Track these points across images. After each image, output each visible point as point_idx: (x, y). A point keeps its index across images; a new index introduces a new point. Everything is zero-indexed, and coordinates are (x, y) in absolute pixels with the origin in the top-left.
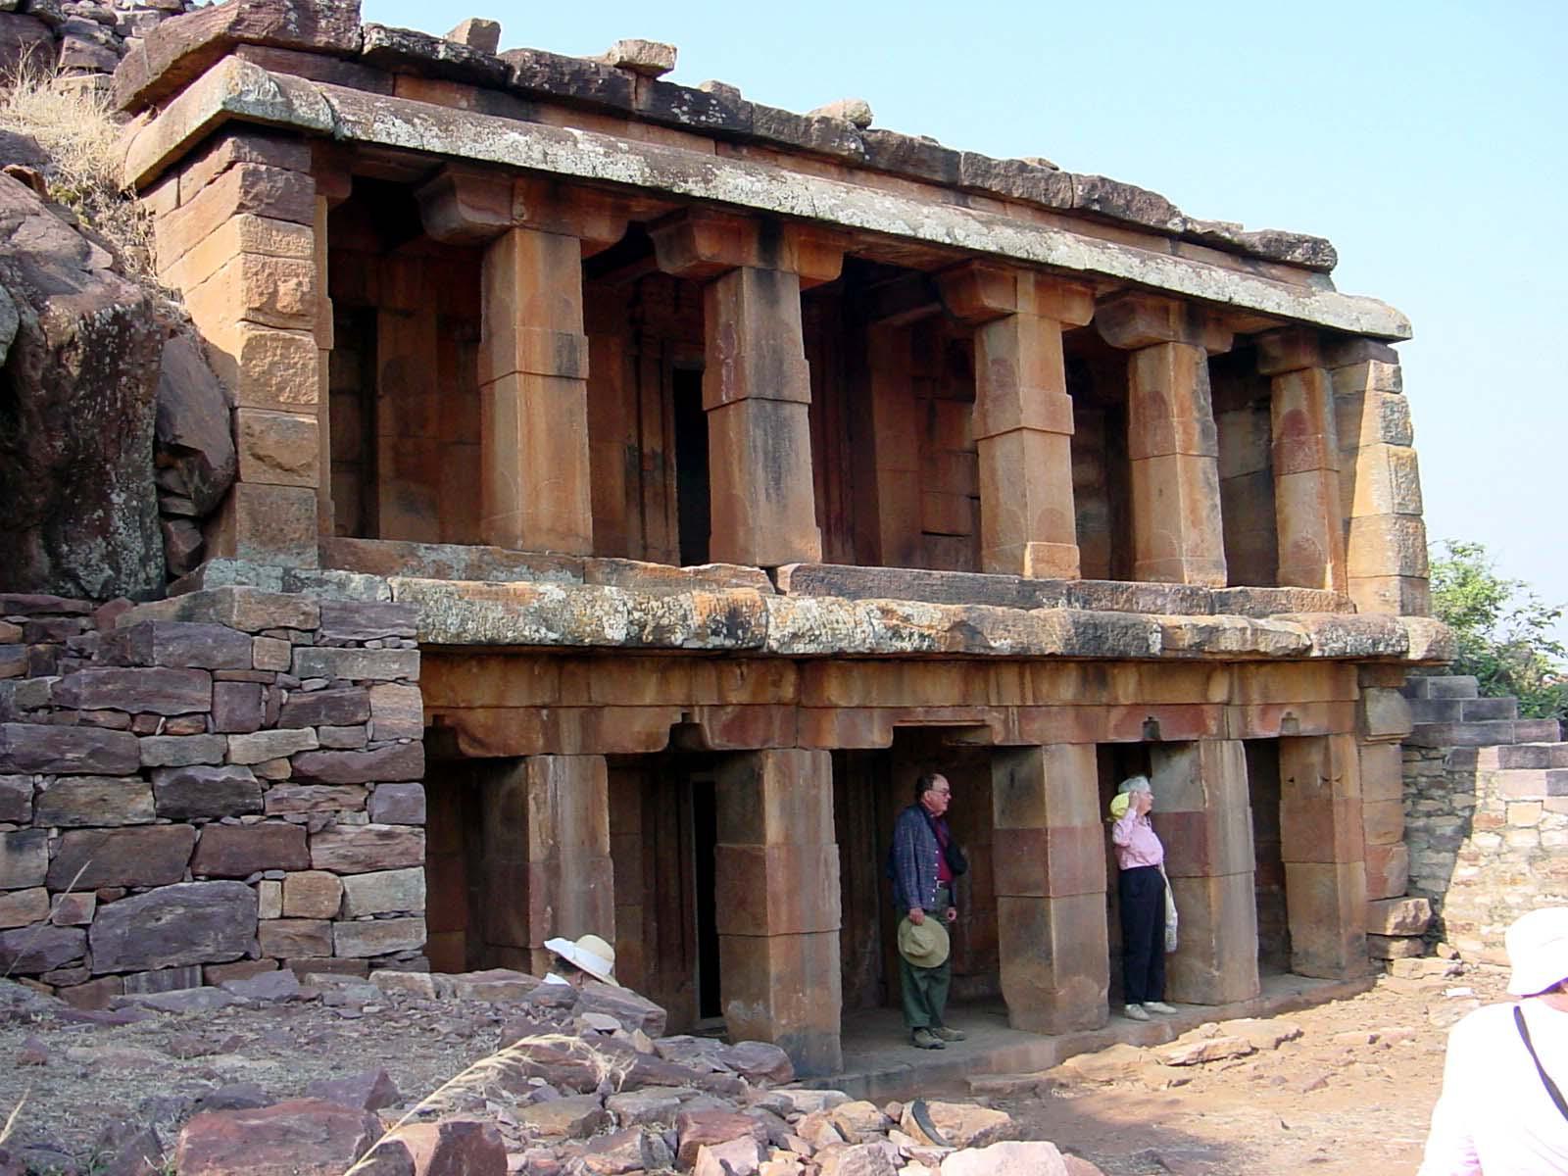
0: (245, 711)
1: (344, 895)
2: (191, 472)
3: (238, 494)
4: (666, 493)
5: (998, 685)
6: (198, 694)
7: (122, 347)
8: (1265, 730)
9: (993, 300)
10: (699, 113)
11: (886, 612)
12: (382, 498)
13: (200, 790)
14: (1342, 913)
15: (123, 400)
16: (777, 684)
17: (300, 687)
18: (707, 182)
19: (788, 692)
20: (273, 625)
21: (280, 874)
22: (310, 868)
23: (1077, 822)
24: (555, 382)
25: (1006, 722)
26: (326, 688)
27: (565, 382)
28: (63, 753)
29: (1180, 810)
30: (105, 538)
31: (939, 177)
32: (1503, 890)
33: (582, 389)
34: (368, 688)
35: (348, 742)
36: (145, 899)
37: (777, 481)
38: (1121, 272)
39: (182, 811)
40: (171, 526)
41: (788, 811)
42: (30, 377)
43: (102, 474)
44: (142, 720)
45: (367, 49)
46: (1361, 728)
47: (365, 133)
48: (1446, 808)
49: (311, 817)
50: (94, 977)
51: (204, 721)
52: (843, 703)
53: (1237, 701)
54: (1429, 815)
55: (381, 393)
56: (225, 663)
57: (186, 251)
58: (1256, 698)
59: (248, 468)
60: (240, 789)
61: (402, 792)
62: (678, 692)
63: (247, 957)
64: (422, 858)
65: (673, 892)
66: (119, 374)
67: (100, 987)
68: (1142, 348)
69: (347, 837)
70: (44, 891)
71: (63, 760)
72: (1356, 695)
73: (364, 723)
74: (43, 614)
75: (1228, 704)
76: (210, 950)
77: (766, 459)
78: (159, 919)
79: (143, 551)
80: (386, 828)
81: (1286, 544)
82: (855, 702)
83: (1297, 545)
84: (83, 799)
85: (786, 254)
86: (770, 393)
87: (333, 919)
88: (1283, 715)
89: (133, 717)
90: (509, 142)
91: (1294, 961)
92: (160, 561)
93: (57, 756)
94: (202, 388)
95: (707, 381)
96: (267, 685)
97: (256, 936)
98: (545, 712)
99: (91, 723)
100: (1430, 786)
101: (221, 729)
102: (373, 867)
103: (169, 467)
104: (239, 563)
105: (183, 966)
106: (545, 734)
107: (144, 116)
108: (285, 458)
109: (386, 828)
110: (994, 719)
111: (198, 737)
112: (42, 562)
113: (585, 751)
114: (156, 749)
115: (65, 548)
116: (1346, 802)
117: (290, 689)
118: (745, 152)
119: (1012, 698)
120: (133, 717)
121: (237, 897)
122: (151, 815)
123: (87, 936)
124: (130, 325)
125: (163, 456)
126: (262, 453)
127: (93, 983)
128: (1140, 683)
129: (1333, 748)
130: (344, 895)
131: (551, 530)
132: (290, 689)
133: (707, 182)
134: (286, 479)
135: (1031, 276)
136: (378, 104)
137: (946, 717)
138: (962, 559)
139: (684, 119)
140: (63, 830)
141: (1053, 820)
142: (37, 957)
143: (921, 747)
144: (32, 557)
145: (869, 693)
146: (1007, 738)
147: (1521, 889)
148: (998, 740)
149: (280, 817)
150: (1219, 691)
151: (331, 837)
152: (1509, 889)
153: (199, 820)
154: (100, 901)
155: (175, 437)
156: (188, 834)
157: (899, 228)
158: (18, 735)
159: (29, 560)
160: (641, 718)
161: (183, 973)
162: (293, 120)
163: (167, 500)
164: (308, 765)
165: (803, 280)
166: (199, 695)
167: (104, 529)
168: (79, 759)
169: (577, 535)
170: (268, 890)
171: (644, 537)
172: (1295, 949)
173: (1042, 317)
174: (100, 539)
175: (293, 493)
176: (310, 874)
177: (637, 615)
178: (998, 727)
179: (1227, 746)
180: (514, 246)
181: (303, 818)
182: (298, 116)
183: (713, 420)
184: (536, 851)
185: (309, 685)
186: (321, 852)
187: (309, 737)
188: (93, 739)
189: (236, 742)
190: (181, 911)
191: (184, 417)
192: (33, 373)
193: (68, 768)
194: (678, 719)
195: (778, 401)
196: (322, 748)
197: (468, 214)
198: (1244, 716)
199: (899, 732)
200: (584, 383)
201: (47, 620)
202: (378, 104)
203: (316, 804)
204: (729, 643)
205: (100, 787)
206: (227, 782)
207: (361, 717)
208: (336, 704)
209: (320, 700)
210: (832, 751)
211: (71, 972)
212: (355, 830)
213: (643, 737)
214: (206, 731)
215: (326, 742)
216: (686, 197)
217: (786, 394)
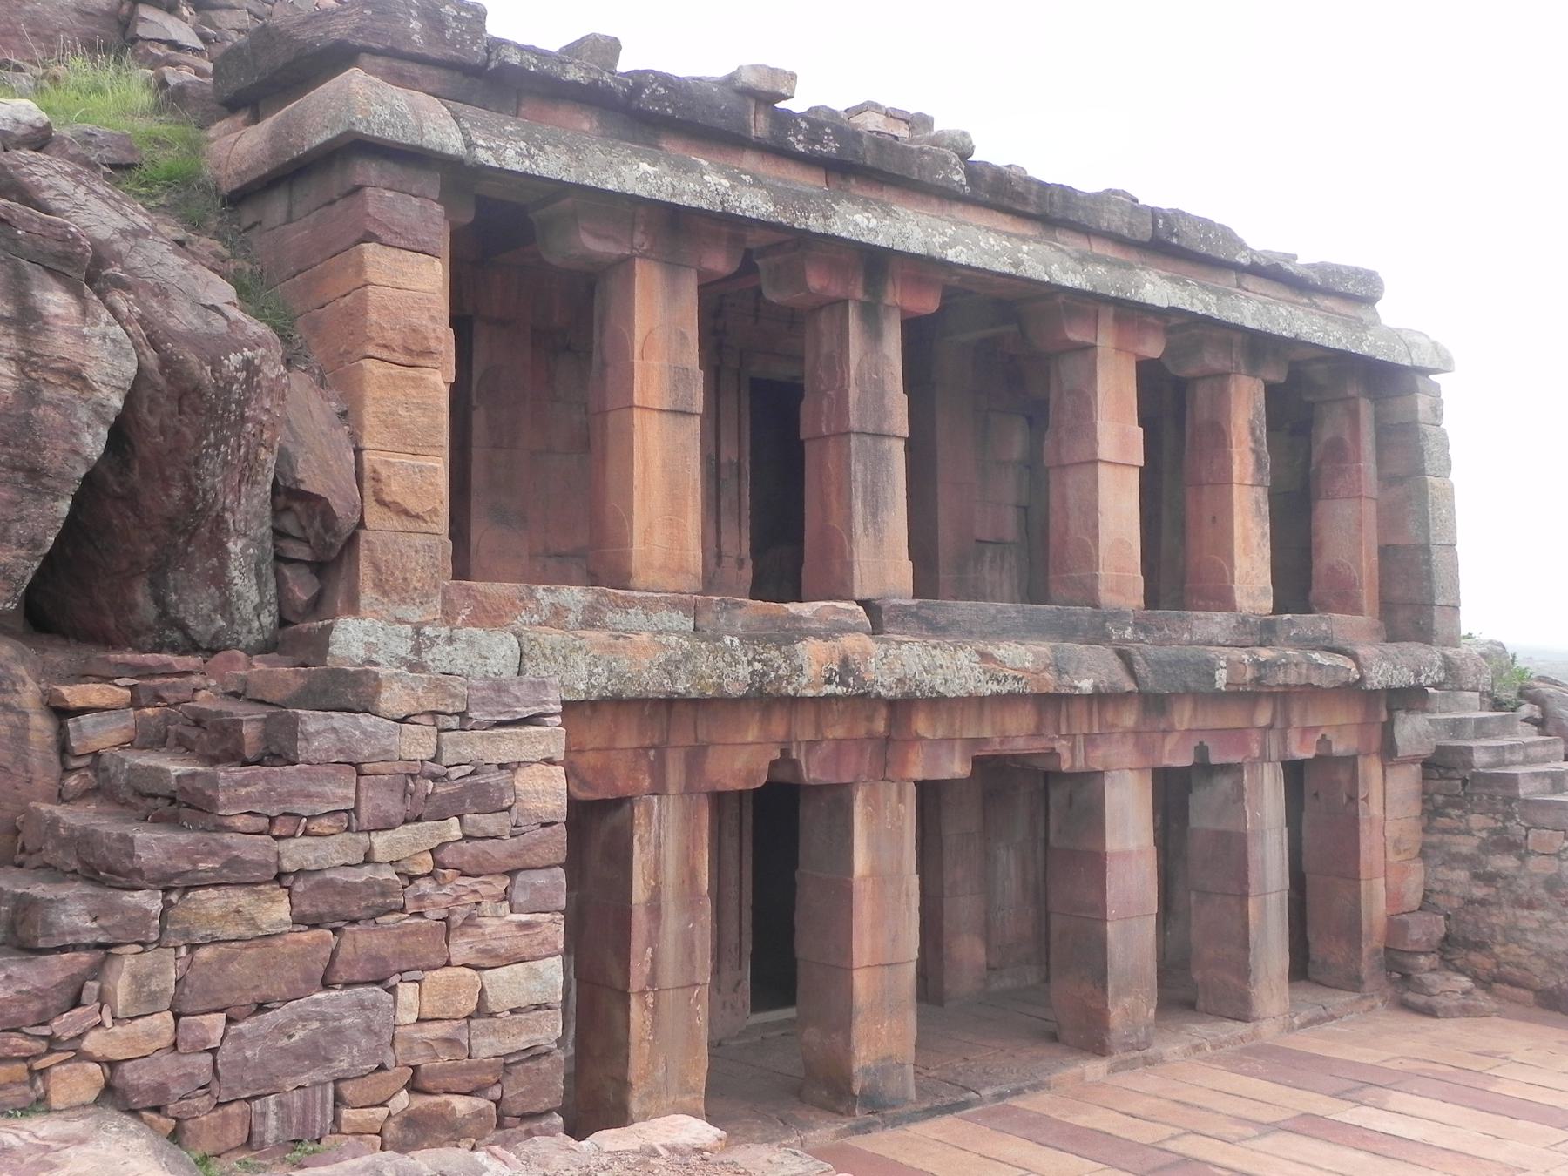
0: (393, 806)
1: (482, 991)
2: (311, 518)
3: (362, 540)
4: (775, 533)
5: (1068, 718)
6: (340, 792)
8: (1302, 751)
9: (1076, 335)
10: (814, 142)
11: (985, 656)
12: (474, 511)
13: (339, 893)
14: (1365, 928)
15: (248, 446)
16: (870, 719)
17: (446, 775)
18: (826, 218)
19: (880, 726)
20: (420, 710)
21: (417, 975)
22: (448, 964)
24: (671, 417)
25: (1072, 750)
26: (472, 774)
27: (681, 419)
28: (195, 863)
29: (1221, 827)
30: (219, 588)
31: (1031, 210)
32: (1519, 912)
33: (695, 424)
34: (514, 771)
35: (492, 830)
36: (279, 1015)
37: (874, 515)
38: (1198, 308)
39: (320, 916)
40: (287, 571)
41: (874, 847)
42: (146, 422)
43: (220, 521)
44: (280, 823)
45: (493, 65)
46: (1388, 752)
47: (497, 160)
48: (1462, 826)
49: (450, 912)
50: (219, 1105)
51: (349, 819)
52: (929, 736)
53: (1279, 725)
54: (1445, 831)
55: (475, 403)
56: (373, 755)
57: (300, 272)
58: (1296, 720)
59: (374, 515)
60: (385, 889)
61: (540, 878)
63: (382, 1067)
64: (561, 946)
66: (243, 419)
67: (225, 1116)
68: (1203, 378)
69: (488, 930)
70: (169, 1015)
71: (196, 871)
73: (508, 809)
74: (152, 675)
76: (345, 1065)
77: (865, 493)
78: (290, 1037)
79: (257, 600)
80: (524, 917)
81: (1320, 565)
82: (940, 734)
83: (1332, 569)
84: (217, 913)
85: (890, 288)
86: (870, 428)
87: (469, 1017)
88: (1319, 737)
89: (272, 820)
90: (639, 174)
91: (1311, 968)
92: (273, 608)
93: (188, 867)
94: (324, 428)
95: (806, 409)
96: (413, 776)
97: (392, 1044)
98: (652, 753)
99: (229, 829)
100: (1447, 804)
101: (365, 827)
103: (287, 509)
104: (366, 623)
105: (315, 1084)
106: (652, 776)
107: (241, 117)
108: (412, 504)
109: (524, 917)
110: (1062, 746)
111: (339, 838)
112: (146, 609)
113: (688, 790)
114: (296, 852)
115: (174, 597)
117: (435, 778)
118: (853, 182)
119: (1081, 727)
120: (272, 820)
121: (374, 1006)
122: (287, 924)
123: (215, 1062)
124: (258, 370)
125: (281, 500)
126: (387, 499)
127: (220, 1111)
128: (1195, 709)
129: (1360, 768)
130: (482, 991)
131: (663, 568)
132: (435, 778)
133: (826, 218)
134: (410, 525)
135: (1111, 310)
136: (508, 128)
137: (1021, 745)
138: (1007, 566)
139: (800, 147)
140: (192, 947)
141: (1112, 844)
142: (161, 1089)
143: (999, 776)
144: (136, 605)
145: (952, 725)
146: (1073, 765)
147: (1539, 914)
148: (1065, 767)
149: (420, 914)
150: (1263, 717)
151: (470, 930)
152: (1526, 913)
153: (336, 924)
154: (229, 1021)
155: (297, 481)
156: (326, 942)
157: (1002, 266)
158: (148, 847)
159: (133, 607)
160: (742, 761)
161: (314, 1093)
162: (425, 144)
163: (283, 544)
165: (903, 311)
166: (340, 792)
167: (219, 579)
168: (213, 869)
169: (688, 572)
170: (407, 993)
171: (718, 545)
172: (1313, 957)
173: (1118, 349)
174: (213, 589)
175: (418, 540)
176: (449, 971)
177: (758, 666)
178: (1066, 755)
179: (1267, 768)
180: (634, 275)
181: (444, 914)
182: (429, 141)
183: (810, 449)
184: (639, 893)
185: (456, 773)
186: (461, 949)
187: (453, 829)
188: (229, 847)
189: (379, 841)
190: (316, 1025)
191: (307, 461)
192: (149, 419)
193: (203, 879)
194: (777, 754)
195: (880, 435)
196: (466, 837)
197: (594, 244)
198: (1284, 738)
199: (978, 762)
200: (697, 419)
201: (158, 681)
202: (508, 128)
203: (457, 898)
204: (840, 690)
206: (369, 884)
207: (506, 803)
208: (481, 792)
209: (465, 788)
210: (916, 783)
211: (196, 1102)
212: (499, 925)
213: (743, 774)
214: (348, 829)
215: (468, 831)
216: (806, 232)
217: (886, 428)
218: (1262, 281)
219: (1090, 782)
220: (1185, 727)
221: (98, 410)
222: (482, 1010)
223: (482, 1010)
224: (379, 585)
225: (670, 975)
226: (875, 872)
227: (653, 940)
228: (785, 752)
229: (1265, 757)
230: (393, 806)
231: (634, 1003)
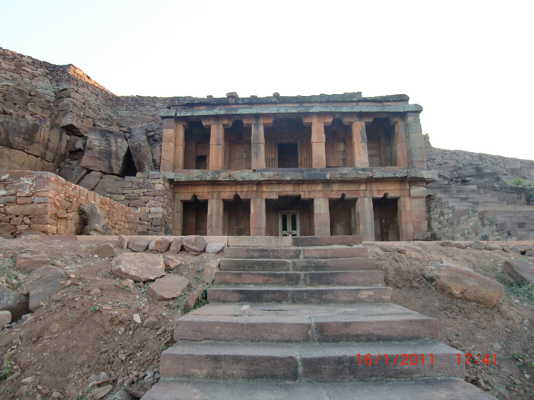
7: (140, 148)
11: (261, 174)
23: (322, 212)
37: (257, 156)
41: (255, 209)
60: (136, 197)
62: (233, 189)
65: (274, 230)
72: (408, 188)
75: (366, 190)
102: (154, 207)
108: (167, 159)
113: (218, 199)
114: (125, 192)
116: (406, 211)
160: (228, 193)
164: (145, 194)
165: (264, 124)
187: (146, 190)
189: (135, 191)
205: (118, 195)
218: (263, 106)
219: (311, 202)
220: (337, 189)
221: (124, 151)
222: (149, 212)
223: (149, 212)
224: (163, 170)
225: (214, 225)
226: (255, 213)
227: (211, 220)
228: (236, 194)
229: (365, 196)
230: (136, 187)
231: (208, 229)
